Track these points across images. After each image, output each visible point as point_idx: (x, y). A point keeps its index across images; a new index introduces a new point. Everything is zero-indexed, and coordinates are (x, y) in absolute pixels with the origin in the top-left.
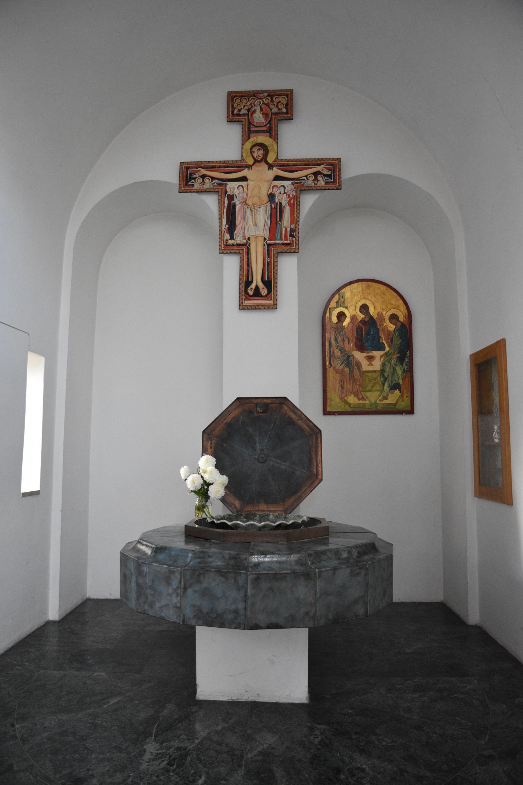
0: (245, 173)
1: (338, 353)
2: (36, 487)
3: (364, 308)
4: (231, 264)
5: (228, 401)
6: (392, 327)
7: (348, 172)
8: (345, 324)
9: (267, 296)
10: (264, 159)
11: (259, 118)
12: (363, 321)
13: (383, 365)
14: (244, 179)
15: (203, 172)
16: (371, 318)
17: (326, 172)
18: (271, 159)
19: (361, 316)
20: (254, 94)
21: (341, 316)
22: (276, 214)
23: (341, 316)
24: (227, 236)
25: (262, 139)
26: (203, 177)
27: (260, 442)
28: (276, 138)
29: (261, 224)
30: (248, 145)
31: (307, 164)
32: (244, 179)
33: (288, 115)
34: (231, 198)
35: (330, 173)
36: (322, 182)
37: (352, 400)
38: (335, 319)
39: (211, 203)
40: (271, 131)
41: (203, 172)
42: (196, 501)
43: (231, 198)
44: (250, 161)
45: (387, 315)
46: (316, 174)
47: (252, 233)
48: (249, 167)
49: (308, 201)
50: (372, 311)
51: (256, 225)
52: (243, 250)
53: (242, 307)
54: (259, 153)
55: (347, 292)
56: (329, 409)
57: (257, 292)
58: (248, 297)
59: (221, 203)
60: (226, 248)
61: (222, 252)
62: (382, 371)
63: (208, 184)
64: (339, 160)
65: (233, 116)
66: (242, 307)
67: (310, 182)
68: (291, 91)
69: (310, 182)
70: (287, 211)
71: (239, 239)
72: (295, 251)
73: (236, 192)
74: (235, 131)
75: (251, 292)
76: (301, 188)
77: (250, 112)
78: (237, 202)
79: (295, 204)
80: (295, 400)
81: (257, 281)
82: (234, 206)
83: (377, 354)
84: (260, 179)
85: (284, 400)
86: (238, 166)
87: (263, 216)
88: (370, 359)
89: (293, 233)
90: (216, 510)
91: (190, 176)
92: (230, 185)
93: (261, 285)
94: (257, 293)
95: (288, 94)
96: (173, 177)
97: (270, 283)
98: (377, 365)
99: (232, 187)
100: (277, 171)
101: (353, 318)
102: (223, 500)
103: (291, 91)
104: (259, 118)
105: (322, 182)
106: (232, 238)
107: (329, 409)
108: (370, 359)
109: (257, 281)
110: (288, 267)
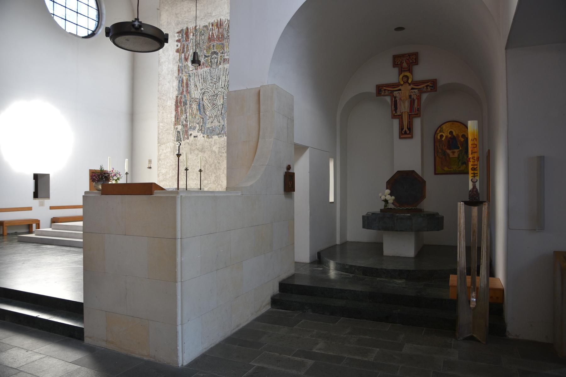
0: (400, 87)
1: (440, 151)
2: (333, 201)
3: (451, 133)
4: (396, 122)
5: (395, 172)
6: (462, 140)
7: (440, 83)
8: (443, 139)
9: (409, 134)
10: (407, 82)
11: (405, 65)
12: (450, 138)
13: (459, 155)
14: (400, 90)
15: (385, 88)
16: (454, 136)
17: (431, 85)
18: (410, 81)
19: (450, 136)
20: (403, 56)
21: (441, 136)
22: (412, 103)
23: (441, 136)
24: (394, 112)
25: (408, 74)
26: (385, 90)
27: (406, 186)
28: (411, 73)
29: (407, 107)
30: (401, 76)
31: (423, 82)
32: (400, 90)
33: (416, 62)
34: (395, 97)
35: (432, 85)
36: (429, 89)
37: (446, 169)
38: (439, 137)
39: (388, 99)
40: (410, 70)
41: (385, 88)
42: (383, 203)
43: (395, 97)
44: (402, 83)
45: (460, 135)
46: (427, 86)
47: (403, 111)
48: (402, 85)
49: (424, 96)
50: (454, 133)
51: (405, 107)
52: (400, 117)
53: (400, 138)
54: (405, 79)
55: (444, 127)
56: (437, 172)
57: (406, 133)
58: (402, 134)
59: (392, 100)
60: (394, 117)
61: (392, 118)
62: (458, 157)
63: (387, 93)
64: (436, 80)
65: (395, 65)
66: (400, 138)
67: (425, 90)
68: (417, 53)
69: (425, 90)
70: (416, 101)
71: (398, 113)
72: (419, 116)
73: (397, 95)
74: (396, 70)
75: (403, 132)
76: (421, 92)
77: (402, 63)
78: (397, 99)
79: (419, 98)
80: (419, 172)
81: (405, 128)
82: (396, 101)
83: (456, 151)
84: (406, 90)
85: (413, 171)
86: (398, 85)
87: (407, 104)
88: (453, 153)
89: (419, 110)
90: (391, 206)
91: (380, 90)
92: (395, 93)
93: (407, 130)
94: (405, 133)
95: (416, 54)
96: (374, 90)
97: (410, 128)
98: (456, 155)
99: (396, 93)
100: (412, 86)
101: (446, 137)
102: (393, 203)
103: (417, 53)
104: (405, 65)
105: (429, 89)
106: (396, 113)
107: (437, 172)
108: (453, 153)
109: (405, 128)
110: (417, 123)
